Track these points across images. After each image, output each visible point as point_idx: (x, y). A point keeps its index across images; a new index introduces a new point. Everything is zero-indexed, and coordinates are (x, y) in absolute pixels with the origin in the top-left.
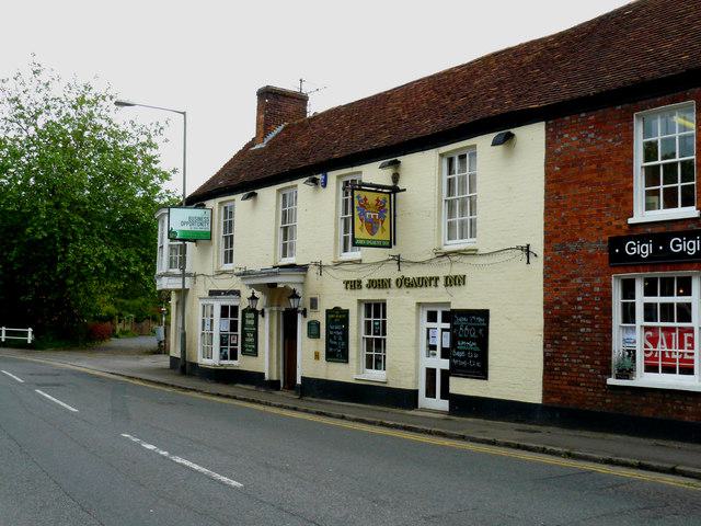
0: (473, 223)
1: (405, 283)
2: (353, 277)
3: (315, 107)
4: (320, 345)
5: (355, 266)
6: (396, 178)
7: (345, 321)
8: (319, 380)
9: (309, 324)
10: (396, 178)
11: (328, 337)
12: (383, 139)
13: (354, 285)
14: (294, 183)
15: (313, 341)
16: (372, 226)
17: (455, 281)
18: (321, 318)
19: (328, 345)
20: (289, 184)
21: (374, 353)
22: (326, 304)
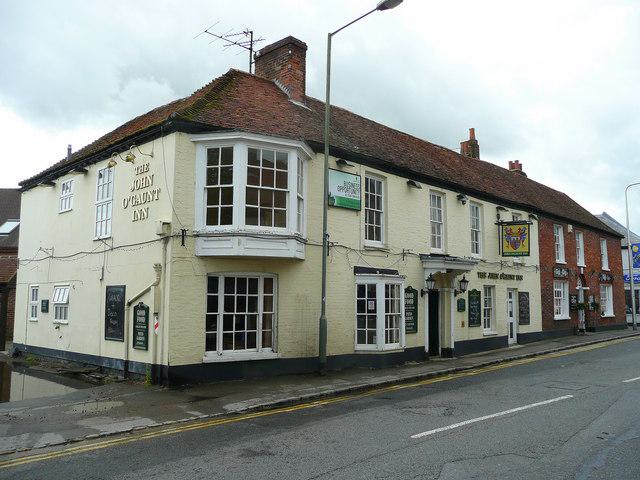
0: (378, 229)
1: (505, 277)
2: (483, 270)
3: (483, 157)
4: (465, 316)
5: (379, 254)
6: (498, 216)
7: (479, 299)
8: (464, 342)
9: (458, 301)
10: (498, 216)
11: (470, 309)
12: (507, 195)
13: (481, 275)
14: (444, 191)
15: (460, 314)
16: (515, 245)
17: (520, 278)
18: (465, 296)
19: (470, 315)
20: (440, 189)
21: (367, 329)
22: (470, 287)
